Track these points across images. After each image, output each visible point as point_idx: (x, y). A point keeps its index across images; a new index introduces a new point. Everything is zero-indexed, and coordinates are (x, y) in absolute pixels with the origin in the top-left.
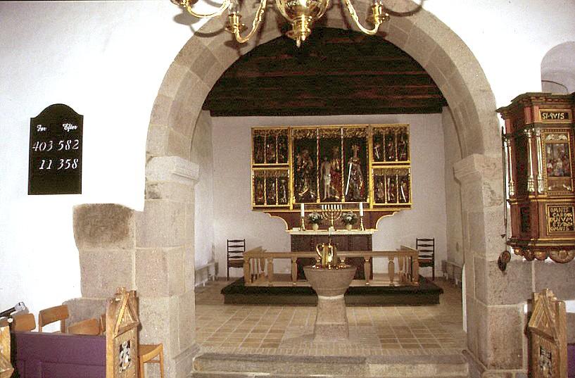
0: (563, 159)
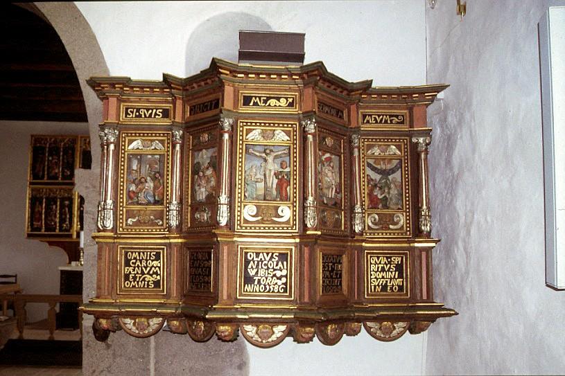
0: (154, 179)
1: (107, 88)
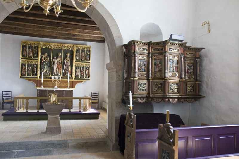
1: (136, 43)
